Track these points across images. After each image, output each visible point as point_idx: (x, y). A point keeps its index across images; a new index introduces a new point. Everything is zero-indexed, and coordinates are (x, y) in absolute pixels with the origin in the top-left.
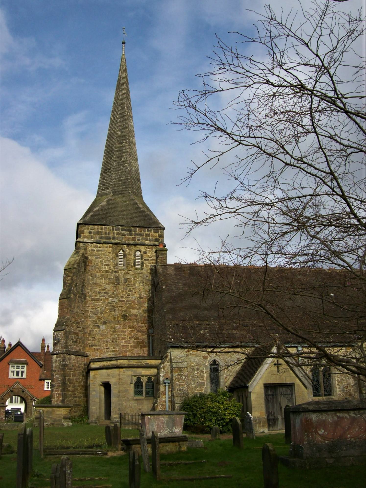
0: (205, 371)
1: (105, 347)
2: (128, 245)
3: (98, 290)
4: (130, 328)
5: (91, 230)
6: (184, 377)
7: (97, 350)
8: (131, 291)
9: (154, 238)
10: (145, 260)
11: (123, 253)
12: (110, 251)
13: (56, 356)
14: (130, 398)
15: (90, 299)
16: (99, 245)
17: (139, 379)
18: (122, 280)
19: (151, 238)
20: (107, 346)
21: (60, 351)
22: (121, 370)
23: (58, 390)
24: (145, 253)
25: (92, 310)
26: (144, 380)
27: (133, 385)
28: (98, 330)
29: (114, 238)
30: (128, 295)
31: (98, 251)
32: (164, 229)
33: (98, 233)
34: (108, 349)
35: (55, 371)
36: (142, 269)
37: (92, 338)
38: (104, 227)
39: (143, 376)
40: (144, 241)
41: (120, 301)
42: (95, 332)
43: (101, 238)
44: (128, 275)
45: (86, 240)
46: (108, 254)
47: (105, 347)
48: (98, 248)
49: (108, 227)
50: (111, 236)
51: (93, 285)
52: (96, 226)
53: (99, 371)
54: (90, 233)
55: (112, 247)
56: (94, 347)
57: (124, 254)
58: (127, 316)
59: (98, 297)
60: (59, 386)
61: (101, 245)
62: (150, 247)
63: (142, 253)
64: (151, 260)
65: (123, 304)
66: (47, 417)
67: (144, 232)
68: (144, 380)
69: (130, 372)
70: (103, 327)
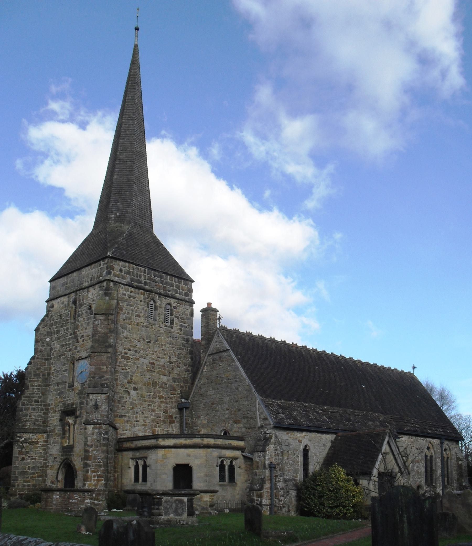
0: (299, 456)
2: (160, 294)
4: (160, 399)
6: (291, 462)
7: (127, 422)
9: (183, 292)
10: (176, 317)
12: (142, 299)
13: (92, 426)
14: (216, 483)
16: (130, 289)
17: (222, 462)
20: (136, 418)
21: (100, 420)
23: (98, 471)
24: (175, 308)
25: (123, 371)
26: (227, 463)
27: (218, 468)
28: (128, 396)
29: (145, 283)
30: (158, 357)
31: (129, 296)
32: (193, 281)
33: (128, 273)
34: (138, 421)
35: (91, 446)
36: (172, 328)
37: (122, 406)
38: (135, 266)
40: (173, 293)
43: (132, 280)
45: (116, 279)
46: (139, 302)
48: (129, 293)
49: (139, 268)
50: (143, 279)
51: (123, 339)
52: (127, 264)
53: (173, 450)
54: (121, 271)
56: (123, 419)
57: (155, 305)
59: (129, 355)
60: (100, 466)
61: (133, 289)
62: (180, 301)
63: (172, 308)
64: (181, 318)
65: (153, 368)
66: (196, 504)
68: (227, 463)
69: (216, 453)
70: (133, 393)
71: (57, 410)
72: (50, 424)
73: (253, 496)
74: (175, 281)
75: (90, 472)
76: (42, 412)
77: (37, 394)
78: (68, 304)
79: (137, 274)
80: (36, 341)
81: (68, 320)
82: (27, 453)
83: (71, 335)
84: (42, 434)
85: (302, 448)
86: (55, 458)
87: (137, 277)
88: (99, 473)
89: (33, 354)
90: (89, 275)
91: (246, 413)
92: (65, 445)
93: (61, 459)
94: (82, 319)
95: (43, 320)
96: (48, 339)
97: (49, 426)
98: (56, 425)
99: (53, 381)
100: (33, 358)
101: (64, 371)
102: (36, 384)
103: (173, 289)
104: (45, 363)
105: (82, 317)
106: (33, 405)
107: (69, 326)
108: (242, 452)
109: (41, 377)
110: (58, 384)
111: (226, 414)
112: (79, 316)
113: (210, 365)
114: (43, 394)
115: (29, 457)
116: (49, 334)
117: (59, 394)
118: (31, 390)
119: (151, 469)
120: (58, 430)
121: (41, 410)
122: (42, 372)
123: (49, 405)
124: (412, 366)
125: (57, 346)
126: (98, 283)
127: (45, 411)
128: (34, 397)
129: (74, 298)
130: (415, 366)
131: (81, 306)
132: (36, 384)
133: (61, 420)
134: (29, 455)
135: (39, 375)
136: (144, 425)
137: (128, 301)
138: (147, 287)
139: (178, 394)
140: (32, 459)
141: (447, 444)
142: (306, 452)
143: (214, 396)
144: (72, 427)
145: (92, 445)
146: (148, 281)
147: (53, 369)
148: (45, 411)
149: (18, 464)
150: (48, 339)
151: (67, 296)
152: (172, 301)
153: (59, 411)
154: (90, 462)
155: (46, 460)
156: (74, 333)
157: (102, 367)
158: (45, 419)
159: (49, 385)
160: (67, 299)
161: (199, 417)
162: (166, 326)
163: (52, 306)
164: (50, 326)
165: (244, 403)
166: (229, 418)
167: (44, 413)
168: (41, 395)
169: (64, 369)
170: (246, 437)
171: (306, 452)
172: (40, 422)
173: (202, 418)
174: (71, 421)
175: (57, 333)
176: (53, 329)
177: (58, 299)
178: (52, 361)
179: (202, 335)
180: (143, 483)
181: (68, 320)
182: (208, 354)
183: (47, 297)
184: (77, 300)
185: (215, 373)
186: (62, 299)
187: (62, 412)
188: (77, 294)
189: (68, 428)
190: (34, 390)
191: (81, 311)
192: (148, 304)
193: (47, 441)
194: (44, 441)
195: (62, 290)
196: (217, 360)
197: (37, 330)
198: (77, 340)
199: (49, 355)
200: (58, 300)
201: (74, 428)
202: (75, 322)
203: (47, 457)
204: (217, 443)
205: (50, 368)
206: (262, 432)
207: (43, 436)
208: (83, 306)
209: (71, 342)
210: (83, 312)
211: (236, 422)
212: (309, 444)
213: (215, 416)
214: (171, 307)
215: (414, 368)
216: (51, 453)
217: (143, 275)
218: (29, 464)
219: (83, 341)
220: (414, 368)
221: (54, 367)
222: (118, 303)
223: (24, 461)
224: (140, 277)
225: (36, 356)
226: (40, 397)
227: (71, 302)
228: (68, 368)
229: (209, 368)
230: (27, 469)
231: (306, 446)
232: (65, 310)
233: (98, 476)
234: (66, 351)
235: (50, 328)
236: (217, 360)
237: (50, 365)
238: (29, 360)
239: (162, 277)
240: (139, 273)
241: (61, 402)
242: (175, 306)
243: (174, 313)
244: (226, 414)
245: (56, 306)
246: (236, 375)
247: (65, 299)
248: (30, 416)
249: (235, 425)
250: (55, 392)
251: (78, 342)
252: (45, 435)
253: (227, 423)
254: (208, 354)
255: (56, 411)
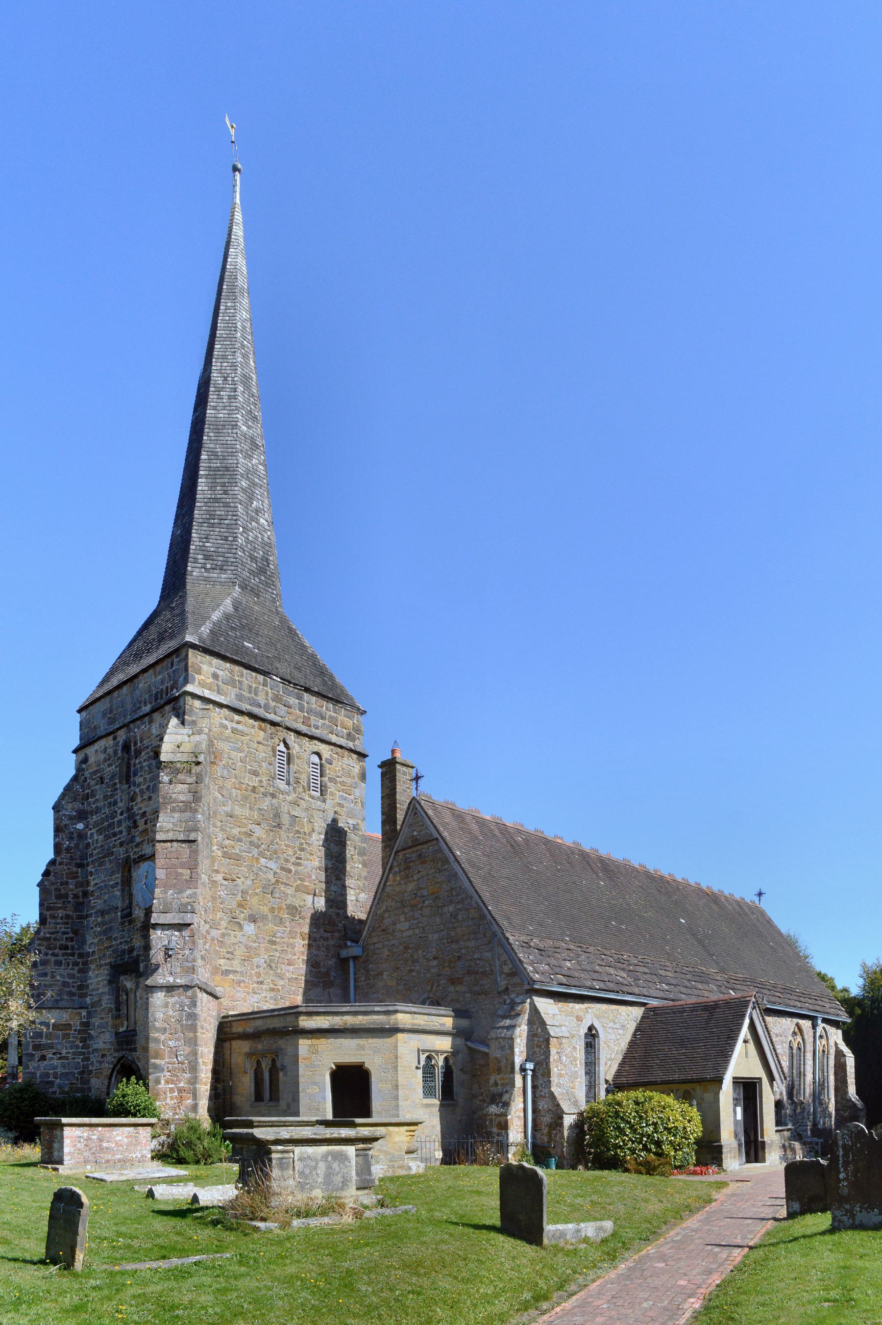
1: (255, 979)
2: (298, 733)
3: (236, 831)
5: (219, 672)
8: (302, 850)
11: (284, 750)
12: (260, 739)
15: (219, 853)
18: (285, 820)
19: (339, 728)
22: (400, 1036)
23: (180, 1081)
25: (226, 883)
27: (420, 1072)
28: (239, 934)
29: (266, 707)
31: (234, 731)
33: (232, 682)
34: (261, 983)
36: (324, 801)
37: (228, 953)
39: (437, 1052)
41: (282, 869)
42: (233, 940)
44: (297, 808)
47: (255, 979)
48: (235, 725)
50: (261, 699)
54: (215, 676)
55: (264, 731)
58: (297, 909)
67: (327, 709)
70: (250, 929)
71: (103, 962)
72: (93, 990)
73: (492, 1127)
74: (327, 708)
75: (163, 1082)
76: (76, 968)
77: (64, 933)
78: (115, 752)
79: (250, 687)
80: (58, 830)
81: (115, 784)
82: (51, 1046)
83: (121, 814)
84: (78, 1011)
85: (584, 1030)
86: (103, 1056)
87: (250, 692)
88: (182, 1085)
89: (51, 855)
90: (153, 688)
91: (473, 964)
92: (121, 1030)
93: (115, 1057)
94: (141, 779)
95: (68, 789)
96: (80, 826)
97: (91, 995)
98: (102, 993)
99: (93, 908)
100: (52, 863)
101: (112, 887)
102: (61, 913)
103: (324, 724)
104: (77, 873)
105: (141, 776)
106: (57, 956)
107: (117, 797)
108: (467, 1040)
109: (70, 899)
110: (102, 913)
111: (433, 967)
112: (135, 775)
113: (400, 872)
114: (76, 932)
115: (54, 1054)
116: (82, 815)
117: (105, 932)
118: (52, 925)
119: (285, 1075)
120: (107, 1001)
121: (73, 965)
122: (71, 890)
123: (88, 954)
124: (756, 891)
125: (96, 838)
126: (168, 702)
127: (81, 966)
128: (58, 940)
129: (124, 737)
130: (763, 891)
131: (138, 753)
132: (61, 913)
133: (110, 982)
134: (54, 1051)
135: (66, 896)
136: (272, 990)
137: (232, 740)
138: (271, 717)
139: (339, 931)
140: (60, 1059)
141: (824, 1028)
142: (592, 1035)
143: (410, 932)
144: (132, 996)
145: (165, 1029)
146: (273, 704)
147: (92, 883)
148: (81, 966)
149: (34, 1068)
150: (80, 826)
151: (111, 737)
152: (324, 749)
153: (106, 964)
154: (163, 1062)
155: (88, 1059)
156: (129, 809)
157: (180, 870)
158: (81, 981)
159: (87, 916)
160: (111, 742)
161: (381, 974)
162: (313, 797)
163: (85, 760)
164: (83, 799)
165: (468, 944)
166: (439, 975)
167: (79, 971)
168: (71, 935)
169: (112, 883)
170: (474, 1010)
171: (592, 1035)
172: (73, 987)
173: (385, 977)
174: (129, 985)
175: (96, 813)
176: (89, 804)
177: (96, 744)
178: (90, 869)
179: (383, 814)
180: (272, 1103)
181: (115, 784)
182: (395, 850)
183: (76, 743)
184: (130, 742)
185: (411, 886)
186: (102, 743)
187: (111, 966)
188: (129, 731)
189: (125, 997)
190: (59, 926)
191: (140, 763)
192: (274, 750)
193: (86, 1025)
194: (83, 1024)
195: (103, 727)
196: (413, 861)
197: (56, 808)
198: (135, 822)
199: (84, 857)
200: (96, 746)
201: (136, 996)
202: (130, 787)
203: (89, 1053)
204: (415, 1021)
205: (88, 883)
206: (505, 1001)
207: (80, 1014)
208: (143, 754)
209: (123, 828)
210: (144, 764)
211: (453, 981)
212: (597, 1025)
213: (411, 971)
214: (321, 759)
215: (760, 894)
216: (95, 1046)
217: (262, 692)
218: (55, 1068)
219: (146, 823)
220: (760, 894)
221: (94, 880)
222: (211, 744)
223: (45, 1063)
224: (256, 694)
225: (59, 859)
226: (72, 939)
227: (120, 748)
228: (119, 881)
229: (398, 878)
230: (51, 1076)
231: (591, 1028)
232: (109, 765)
233: (180, 1090)
234: (114, 846)
235: (83, 804)
236: (413, 861)
237: (87, 877)
238: (44, 868)
239: (300, 698)
240: (254, 685)
241: (110, 947)
242: (328, 757)
243: (327, 771)
244: (433, 967)
245: (92, 759)
246: (452, 889)
247: (109, 742)
248: (53, 977)
249: (451, 988)
250: (99, 929)
251: (136, 826)
252: (84, 1013)
253: (436, 985)
254: (395, 850)
255: (101, 966)
